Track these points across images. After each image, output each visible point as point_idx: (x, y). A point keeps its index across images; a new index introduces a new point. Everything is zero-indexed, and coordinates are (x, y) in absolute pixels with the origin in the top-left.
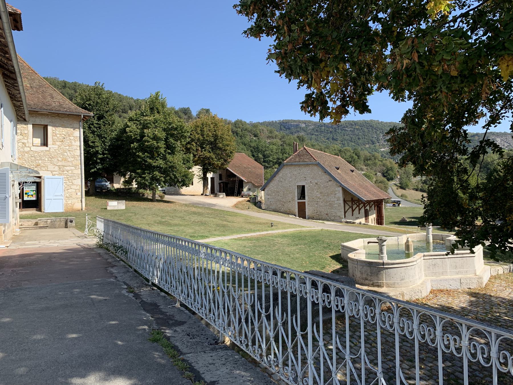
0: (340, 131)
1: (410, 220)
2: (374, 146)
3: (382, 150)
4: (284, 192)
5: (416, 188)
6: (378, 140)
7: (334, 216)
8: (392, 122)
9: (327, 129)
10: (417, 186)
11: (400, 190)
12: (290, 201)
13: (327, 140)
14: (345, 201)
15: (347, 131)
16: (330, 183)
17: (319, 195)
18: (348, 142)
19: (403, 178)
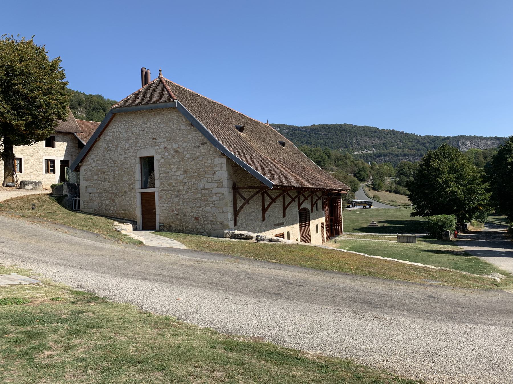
0: (314, 135)
1: (382, 224)
2: (348, 150)
3: (356, 153)
4: (114, 171)
5: (389, 189)
6: (351, 144)
7: (212, 223)
8: (365, 126)
9: (301, 133)
10: (390, 187)
11: (372, 191)
12: (125, 192)
13: (301, 144)
14: (236, 190)
15: (321, 134)
16: (203, 149)
17: (181, 177)
18: (322, 145)
19: (376, 179)
